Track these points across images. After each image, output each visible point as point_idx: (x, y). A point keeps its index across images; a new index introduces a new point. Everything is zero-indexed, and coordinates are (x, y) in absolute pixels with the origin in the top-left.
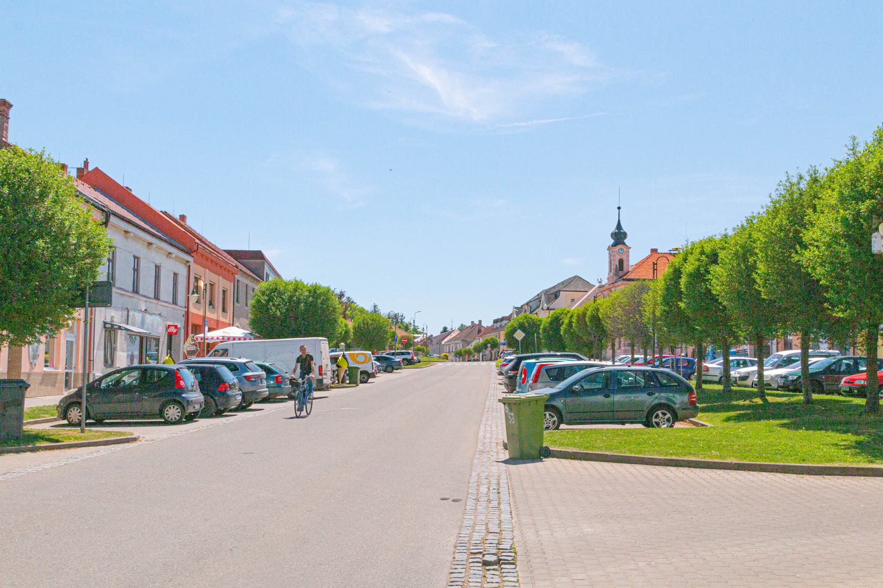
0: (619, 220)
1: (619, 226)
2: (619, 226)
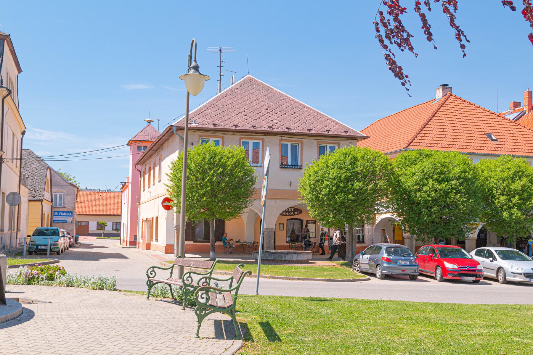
0: (199, 326)
1: (200, 321)
2: (200, 321)
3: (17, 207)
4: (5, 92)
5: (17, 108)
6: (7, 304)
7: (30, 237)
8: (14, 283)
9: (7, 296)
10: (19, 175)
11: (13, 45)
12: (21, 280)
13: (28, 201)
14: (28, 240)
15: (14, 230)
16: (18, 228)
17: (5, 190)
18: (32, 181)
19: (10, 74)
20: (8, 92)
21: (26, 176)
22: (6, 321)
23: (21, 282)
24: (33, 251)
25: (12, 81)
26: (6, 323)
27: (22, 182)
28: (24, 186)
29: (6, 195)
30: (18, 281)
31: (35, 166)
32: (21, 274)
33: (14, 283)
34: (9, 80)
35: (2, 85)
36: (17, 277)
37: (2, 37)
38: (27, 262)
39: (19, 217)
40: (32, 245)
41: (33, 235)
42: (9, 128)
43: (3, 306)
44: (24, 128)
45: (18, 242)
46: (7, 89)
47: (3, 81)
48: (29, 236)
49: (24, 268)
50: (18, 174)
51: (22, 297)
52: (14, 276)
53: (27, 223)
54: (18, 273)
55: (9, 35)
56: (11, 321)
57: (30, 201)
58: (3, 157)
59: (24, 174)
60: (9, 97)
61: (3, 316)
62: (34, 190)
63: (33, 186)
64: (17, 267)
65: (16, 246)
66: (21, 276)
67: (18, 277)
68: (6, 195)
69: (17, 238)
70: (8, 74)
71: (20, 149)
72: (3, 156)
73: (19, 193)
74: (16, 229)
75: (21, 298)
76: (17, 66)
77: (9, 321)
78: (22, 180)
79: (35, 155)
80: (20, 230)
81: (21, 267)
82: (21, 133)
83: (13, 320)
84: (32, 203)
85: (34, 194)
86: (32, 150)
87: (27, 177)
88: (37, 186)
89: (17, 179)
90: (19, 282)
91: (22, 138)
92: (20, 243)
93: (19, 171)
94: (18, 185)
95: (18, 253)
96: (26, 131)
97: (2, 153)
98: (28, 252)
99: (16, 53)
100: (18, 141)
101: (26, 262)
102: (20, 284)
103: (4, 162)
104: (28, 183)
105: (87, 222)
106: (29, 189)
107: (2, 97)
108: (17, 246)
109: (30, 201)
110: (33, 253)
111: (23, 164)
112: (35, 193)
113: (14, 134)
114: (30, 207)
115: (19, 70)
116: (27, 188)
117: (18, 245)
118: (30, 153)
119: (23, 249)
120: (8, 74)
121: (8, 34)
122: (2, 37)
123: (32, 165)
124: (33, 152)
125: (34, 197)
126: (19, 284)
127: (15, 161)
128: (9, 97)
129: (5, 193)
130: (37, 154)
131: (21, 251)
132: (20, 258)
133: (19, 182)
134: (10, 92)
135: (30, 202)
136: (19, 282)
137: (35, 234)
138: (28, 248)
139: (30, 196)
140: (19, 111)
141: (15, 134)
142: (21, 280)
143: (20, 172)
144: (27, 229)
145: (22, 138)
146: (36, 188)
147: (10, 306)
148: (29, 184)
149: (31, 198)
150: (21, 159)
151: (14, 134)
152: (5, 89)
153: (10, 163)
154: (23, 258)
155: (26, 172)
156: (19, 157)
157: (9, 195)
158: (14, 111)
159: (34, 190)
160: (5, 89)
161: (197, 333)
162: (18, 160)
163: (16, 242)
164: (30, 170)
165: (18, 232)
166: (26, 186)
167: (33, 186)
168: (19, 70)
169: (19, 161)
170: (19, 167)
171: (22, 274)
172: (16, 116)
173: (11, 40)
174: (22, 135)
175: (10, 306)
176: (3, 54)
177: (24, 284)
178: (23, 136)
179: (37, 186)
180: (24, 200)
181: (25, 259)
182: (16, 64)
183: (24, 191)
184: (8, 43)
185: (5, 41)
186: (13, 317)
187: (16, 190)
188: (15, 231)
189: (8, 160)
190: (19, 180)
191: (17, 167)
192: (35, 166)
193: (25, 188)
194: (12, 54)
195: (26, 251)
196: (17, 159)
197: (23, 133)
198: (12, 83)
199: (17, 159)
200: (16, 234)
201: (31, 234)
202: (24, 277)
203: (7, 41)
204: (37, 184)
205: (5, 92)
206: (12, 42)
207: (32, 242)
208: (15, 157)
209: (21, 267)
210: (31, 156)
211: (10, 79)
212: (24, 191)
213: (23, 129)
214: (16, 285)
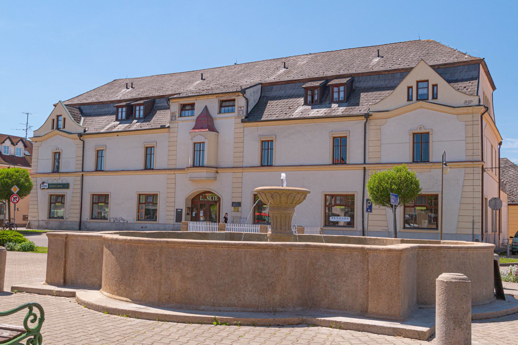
3: (498, 211)
4: (483, 109)
5: (493, 121)
6: (506, 299)
7: (512, 239)
8: (505, 280)
9: (506, 292)
10: (498, 181)
11: (487, 67)
12: (512, 278)
13: (507, 205)
14: (511, 241)
15: (496, 231)
16: (500, 230)
17: (487, 196)
18: (510, 187)
19: (486, 93)
20: (485, 109)
21: (505, 183)
22: (508, 315)
23: (512, 280)
24: (516, 252)
25: (488, 99)
26: (507, 316)
27: (501, 189)
28: (504, 192)
29: (488, 200)
30: (509, 279)
31: (512, 173)
32: (511, 273)
33: (505, 280)
34: (485, 98)
35: (480, 104)
36: (508, 275)
37: (478, 61)
38: (512, 261)
39: (500, 220)
40: (515, 246)
41: (515, 237)
42: (487, 139)
43: (503, 301)
44: (501, 139)
45: (501, 243)
46: (485, 107)
47: (481, 100)
48: (511, 237)
49: (514, 267)
50: (498, 181)
51: (516, 294)
52: (505, 274)
53: (508, 225)
54: (509, 272)
55: (484, 58)
56: (512, 315)
57: (509, 205)
58: (484, 167)
59: (502, 181)
60: (486, 113)
61: (505, 310)
62: (513, 195)
63: (511, 192)
64: (508, 265)
65: (499, 246)
66: (511, 274)
67: (509, 275)
68: (488, 200)
69: (499, 239)
70: (484, 93)
71: (498, 158)
72: (484, 166)
73: (499, 198)
74: (498, 230)
75: (515, 295)
76: (491, 85)
77: (510, 315)
78: (501, 186)
79: (511, 162)
80: (501, 232)
81: (511, 266)
82: (498, 144)
83: (514, 315)
84: (511, 207)
85: (513, 199)
86: (509, 159)
87: (506, 184)
88: (515, 191)
89: (497, 185)
90: (510, 280)
91: (499, 149)
92: (503, 244)
93: (498, 178)
94: (498, 191)
95: (502, 252)
96: (502, 142)
97: (483, 163)
98: (511, 253)
99: (490, 73)
100: (496, 152)
101: (511, 262)
102: (511, 282)
103: (485, 171)
104: (507, 188)
105: (420, 100)
106: (508, 194)
107: (481, 114)
108: (500, 246)
109: (509, 205)
110: (516, 253)
111: (501, 171)
112: (513, 197)
113: (492, 146)
114: (510, 211)
115: (494, 88)
116: (506, 193)
117: (500, 245)
118: (507, 161)
119: (507, 249)
120: (484, 93)
121: (482, 58)
122: (478, 61)
123: (509, 172)
124: (509, 160)
125: (513, 201)
126: (510, 281)
127: (494, 169)
128: (486, 113)
129: (487, 199)
130: (513, 162)
131: (505, 250)
132: (505, 258)
133: (498, 188)
134: (487, 109)
135: (509, 206)
136: (510, 280)
137: (517, 235)
138: (511, 248)
139: (509, 200)
140: (495, 124)
141: (493, 146)
142: (512, 278)
143: (499, 179)
144: (508, 230)
145: (499, 148)
146: (515, 193)
147: (509, 302)
148: (508, 189)
149: (510, 203)
150: (499, 168)
151: (492, 146)
152: (483, 107)
153: (490, 172)
154: (508, 257)
155: (504, 179)
156: (497, 166)
157: (491, 200)
158: (490, 123)
159: (513, 195)
160: (483, 107)
161: (509, 314)
162: (497, 169)
163: (499, 242)
164: (507, 177)
165: (500, 234)
166: (505, 191)
167: (511, 192)
168: (494, 88)
169: (497, 170)
170: (498, 175)
171: (512, 272)
172: (491, 126)
173: (485, 63)
174: (499, 146)
175: (509, 302)
176: (479, 76)
177: (515, 282)
178: (500, 147)
179: (515, 191)
180: (505, 204)
181: (509, 259)
182: (490, 83)
183: (504, 197)
184: (483, 66)
185: (480, 64)
186: (513, 312)
187: (497, 196)
188: (498, 233)
189: (489, 169)
190: (498, 187)
191: (493, 171)
192: (512, 173)
193: (504, 194)
194: (487, 75)
195: (510, 251)
196: (496, 168)
197: (500, 144)
198: (488, 100)
199: (496, 168)
200: (498, 235)
201: (513, 236)
202: (515, 275)
203: (482, 65)
204: (515, 189)
205: (483, 109)
206: (487, 64)
207: (515, 243)
208: (494, 166)
209: (511, 266)
210: (508, 164)
211: (486, 97)
212: (504, 197)
213: (500, 140)
214: (507, 282)
